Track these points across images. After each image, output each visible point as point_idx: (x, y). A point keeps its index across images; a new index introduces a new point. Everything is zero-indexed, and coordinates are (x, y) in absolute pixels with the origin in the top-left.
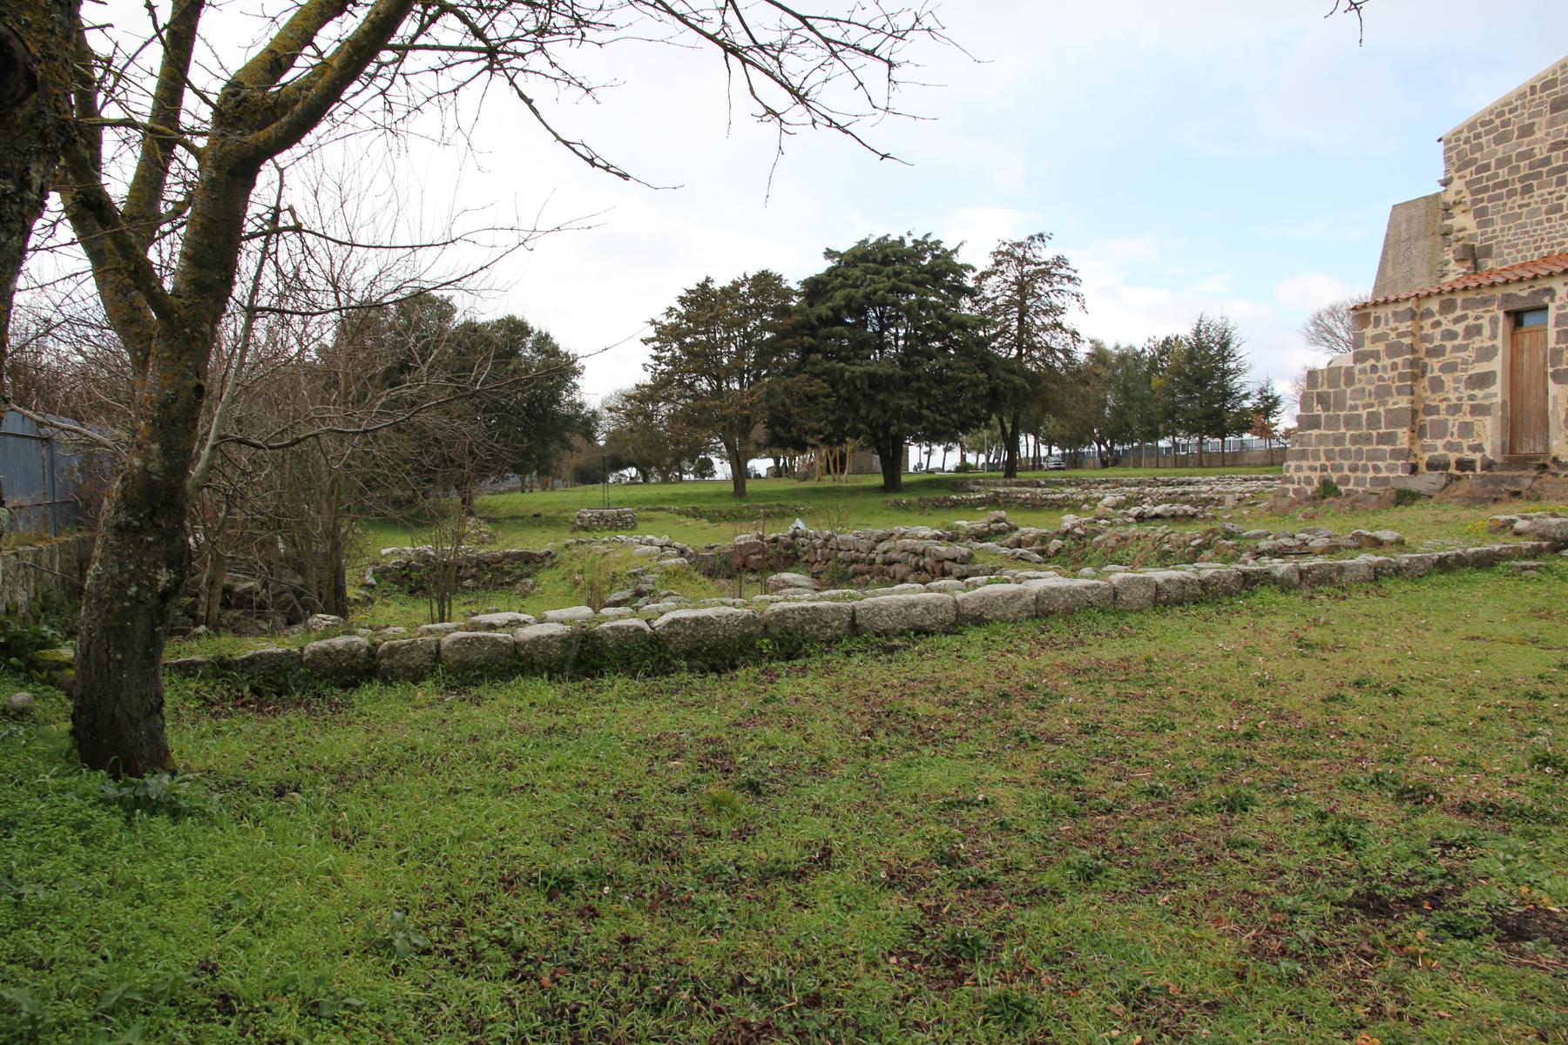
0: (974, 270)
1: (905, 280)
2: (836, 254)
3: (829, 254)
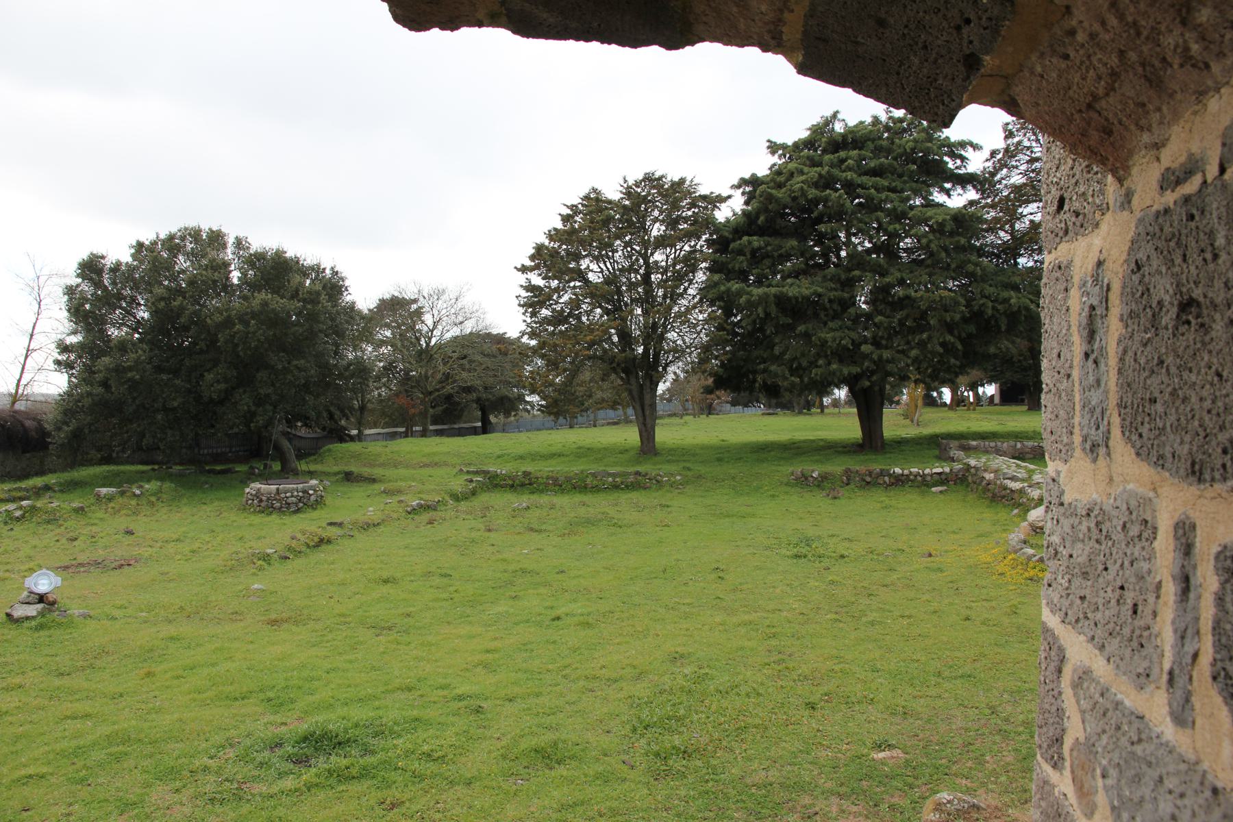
0: (976, 147)
1: (849, 169)
2: (784, 147)
3: (773, 148)
